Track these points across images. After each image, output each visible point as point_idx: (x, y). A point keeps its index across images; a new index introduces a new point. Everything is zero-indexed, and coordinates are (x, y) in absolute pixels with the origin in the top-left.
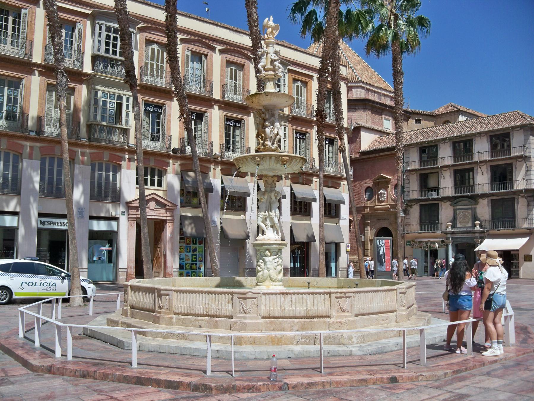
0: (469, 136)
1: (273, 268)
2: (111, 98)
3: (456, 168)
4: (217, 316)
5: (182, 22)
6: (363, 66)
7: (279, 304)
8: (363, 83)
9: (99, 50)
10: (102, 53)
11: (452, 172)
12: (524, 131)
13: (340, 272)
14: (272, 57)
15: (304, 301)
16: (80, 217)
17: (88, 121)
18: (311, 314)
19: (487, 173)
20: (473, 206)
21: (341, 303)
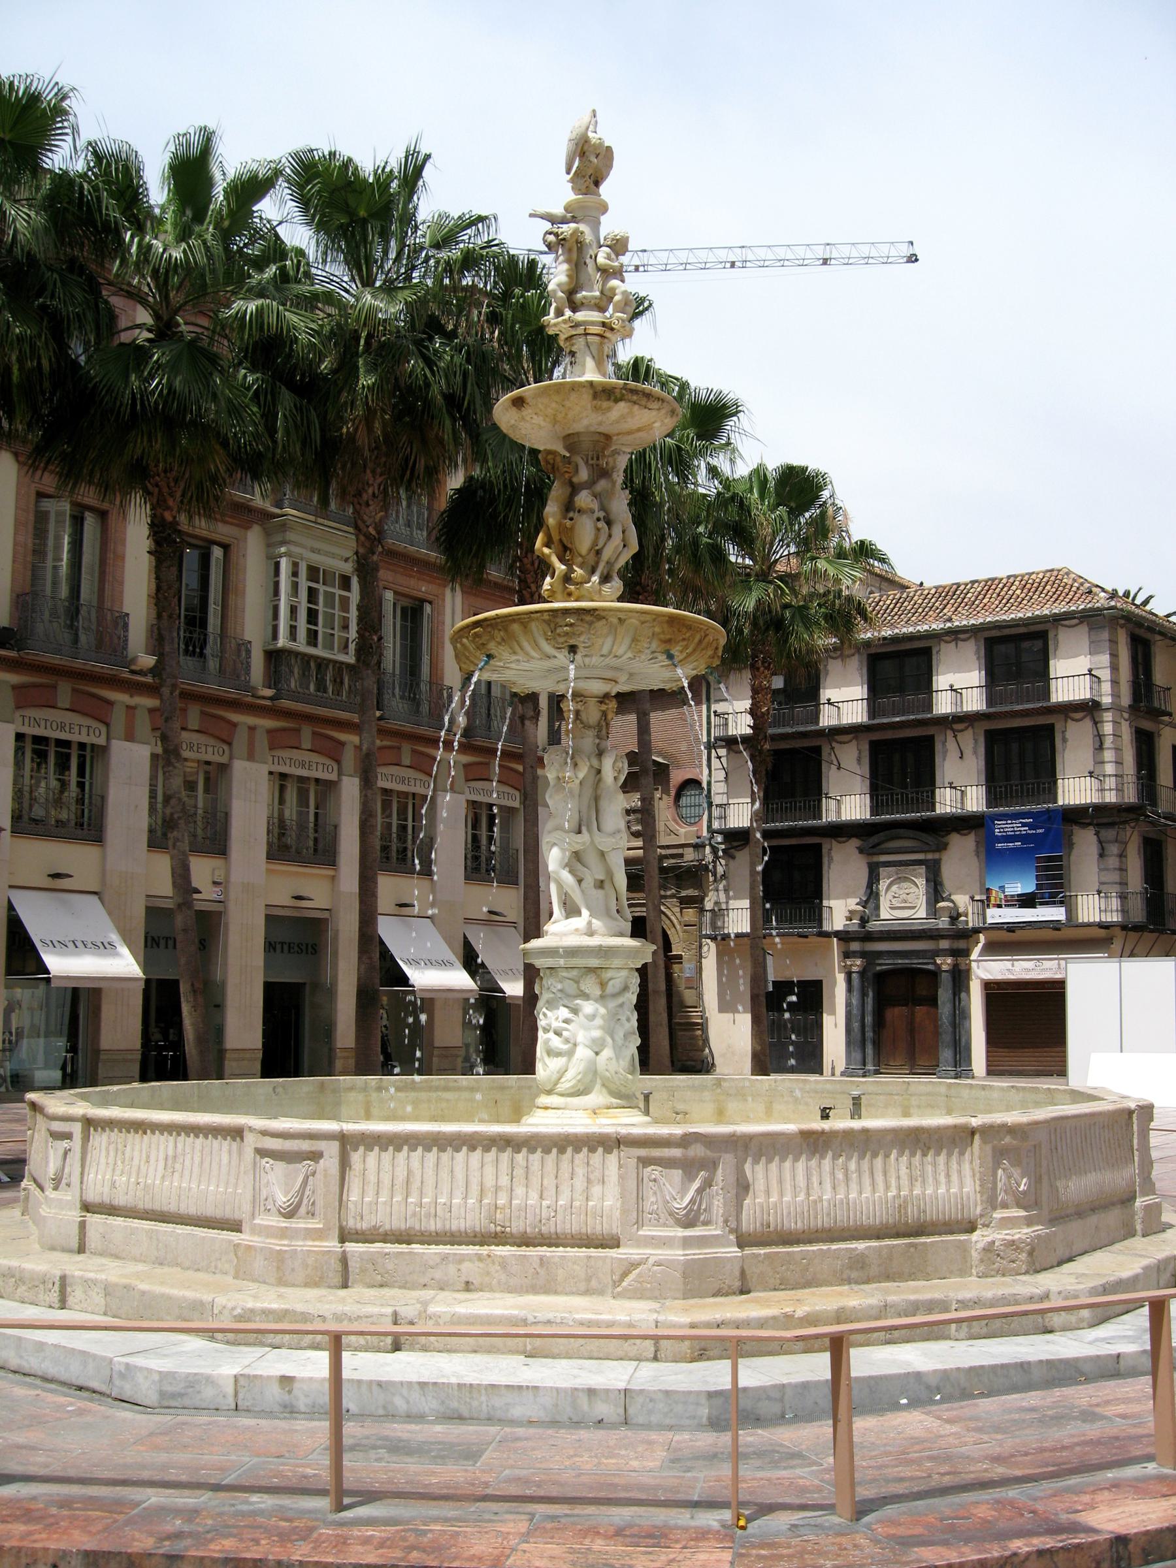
0: (1040, 623)
3: (877, 736)
4: (920, 1230)
11: (866, 747)
12: (1091, 629)
19: (975, 753)
20: (930, 856)
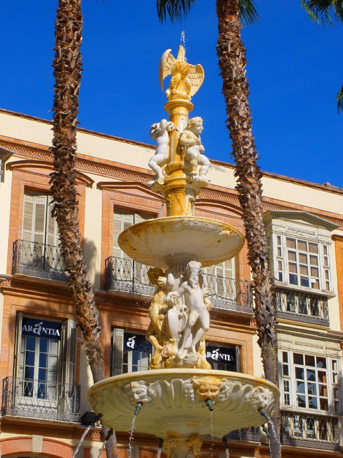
5: (88, 144)
14: (184, 139)
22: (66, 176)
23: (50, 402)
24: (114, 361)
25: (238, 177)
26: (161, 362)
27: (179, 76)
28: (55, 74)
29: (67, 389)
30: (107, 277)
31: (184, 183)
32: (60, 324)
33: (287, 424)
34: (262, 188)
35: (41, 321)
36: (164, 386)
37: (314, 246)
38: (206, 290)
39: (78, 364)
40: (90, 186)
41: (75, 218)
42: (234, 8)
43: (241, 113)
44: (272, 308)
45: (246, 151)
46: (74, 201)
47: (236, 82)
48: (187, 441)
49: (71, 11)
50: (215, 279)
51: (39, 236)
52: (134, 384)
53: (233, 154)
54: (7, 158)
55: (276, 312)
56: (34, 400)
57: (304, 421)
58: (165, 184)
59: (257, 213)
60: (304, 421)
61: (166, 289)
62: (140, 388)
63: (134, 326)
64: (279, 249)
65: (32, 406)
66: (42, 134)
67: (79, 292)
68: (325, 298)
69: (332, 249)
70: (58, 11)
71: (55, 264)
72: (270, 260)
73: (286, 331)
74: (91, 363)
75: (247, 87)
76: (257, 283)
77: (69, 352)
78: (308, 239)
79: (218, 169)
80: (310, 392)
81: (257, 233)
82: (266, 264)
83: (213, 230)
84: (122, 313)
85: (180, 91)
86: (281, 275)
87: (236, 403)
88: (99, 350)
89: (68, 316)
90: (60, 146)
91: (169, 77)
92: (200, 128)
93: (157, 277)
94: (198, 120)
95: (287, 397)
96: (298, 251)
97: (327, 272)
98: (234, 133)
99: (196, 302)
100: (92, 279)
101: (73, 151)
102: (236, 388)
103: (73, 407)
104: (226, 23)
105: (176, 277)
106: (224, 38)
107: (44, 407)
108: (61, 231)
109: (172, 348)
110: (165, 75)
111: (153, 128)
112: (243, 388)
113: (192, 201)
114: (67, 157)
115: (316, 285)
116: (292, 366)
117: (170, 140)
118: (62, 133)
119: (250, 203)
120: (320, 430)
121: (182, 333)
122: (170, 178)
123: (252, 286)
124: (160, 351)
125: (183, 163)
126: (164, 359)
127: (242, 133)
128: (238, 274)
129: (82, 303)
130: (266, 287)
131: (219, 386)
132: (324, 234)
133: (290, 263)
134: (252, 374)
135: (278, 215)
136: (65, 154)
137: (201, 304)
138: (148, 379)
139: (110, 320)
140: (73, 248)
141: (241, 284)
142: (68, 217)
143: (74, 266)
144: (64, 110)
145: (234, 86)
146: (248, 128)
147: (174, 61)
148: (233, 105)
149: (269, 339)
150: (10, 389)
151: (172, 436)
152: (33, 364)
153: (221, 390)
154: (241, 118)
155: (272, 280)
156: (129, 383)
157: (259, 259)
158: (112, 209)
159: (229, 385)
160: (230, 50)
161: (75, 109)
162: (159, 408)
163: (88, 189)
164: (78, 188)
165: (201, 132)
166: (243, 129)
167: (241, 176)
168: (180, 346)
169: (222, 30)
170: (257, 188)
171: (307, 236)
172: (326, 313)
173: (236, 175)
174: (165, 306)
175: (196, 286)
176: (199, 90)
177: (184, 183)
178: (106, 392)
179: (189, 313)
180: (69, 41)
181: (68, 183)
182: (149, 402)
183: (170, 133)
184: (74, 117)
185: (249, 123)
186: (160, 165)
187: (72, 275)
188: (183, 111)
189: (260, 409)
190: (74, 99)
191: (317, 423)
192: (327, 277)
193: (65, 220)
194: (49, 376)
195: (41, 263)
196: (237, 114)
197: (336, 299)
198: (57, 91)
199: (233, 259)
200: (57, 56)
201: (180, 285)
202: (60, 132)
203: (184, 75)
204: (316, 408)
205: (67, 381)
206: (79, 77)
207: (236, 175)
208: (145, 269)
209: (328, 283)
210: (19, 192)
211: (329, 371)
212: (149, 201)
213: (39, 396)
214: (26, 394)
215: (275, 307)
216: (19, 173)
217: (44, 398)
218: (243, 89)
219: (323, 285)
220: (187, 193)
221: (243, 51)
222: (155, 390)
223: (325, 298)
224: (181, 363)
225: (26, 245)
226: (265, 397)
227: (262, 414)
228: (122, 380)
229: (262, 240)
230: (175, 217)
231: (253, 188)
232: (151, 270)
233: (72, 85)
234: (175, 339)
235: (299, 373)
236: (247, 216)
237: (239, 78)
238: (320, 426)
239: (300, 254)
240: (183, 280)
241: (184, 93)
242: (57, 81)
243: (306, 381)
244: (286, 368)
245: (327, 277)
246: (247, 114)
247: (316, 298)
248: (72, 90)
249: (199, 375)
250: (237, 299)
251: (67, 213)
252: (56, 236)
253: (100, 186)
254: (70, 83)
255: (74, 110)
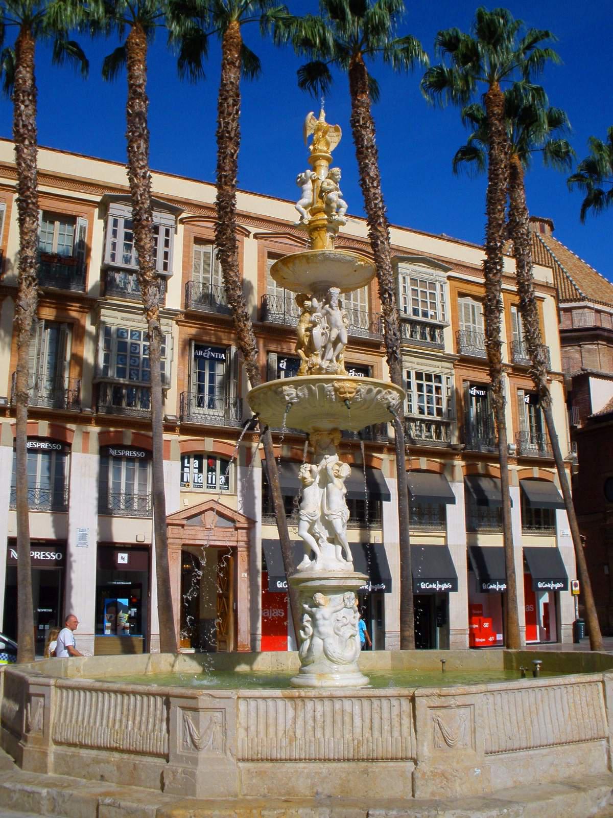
1: (332, 633)
2: (134, 337)
5: (245, 202)
6: (588, 274)
7: (281, 728)
8: (590, 300)
9: (113, 257)
10: (119, 263)
13: (388, 641)
14: (325, 185)
15: (347, 719)
16: (80, 543)
17: (94, 378)
18: (364, 752)
21: (443, 724)
22: (228, 226)
23: (219, 412)
24: (268, 373)
25: (370, 227)
26: (307, 371)
27: (320, 133)
28: (218, 142)
29: (232, 401)
30: (263, 311)
31: (326, 223)
32: (225, 349)
33: (410, 428)
34: (390, 236)
35: (209, 347)
36: (310, 390)
37: (432, 285)
38: (344, 312)
39: (240, 381)
40: (248, 236)
41: (236, 261)
42: (364, 88)
43: (372, 174)
44: (398, 333)
45: (376, 204)
46: (234, 246)
47: (367, 148)
48: (329, 434)
49: (231, 90)
50: (351, 312)
51: (206, 277)
52: (285, 388)
53: (366, 207)
54: (180, 214)
55: (401, 338)
56: (205, 410)
57: (423, 425)
58: (309, 224)
59: (386, 256)
60: (423, 425)
61: (311, 311)
62: (290, 392)
63: (285, 351)
64: (404, 287)
65: (204, 414)
66: (208, 194)
67: (240, 321)
68: (441, 327)
69: (447, 288)
70: (220, 90)
71: (220, 299)
72: (396, 294)
73: (409, 354)
74: (251, 379)
75: (376, 153)
76: (386, 314)
77: (233, 371)
78: (428, 279)
79: (354, 222)
80: (428, 403)
81: (386, 272)
82: (393, 298)
83: (350, 261)
84: (274, 340)
85: (321, 146)
86: (405, 308)
87: (370, 403)
88: (257, 368)
89: (231, 343)
90: (222, 201)
91: (312, 135)
92: (339, 177)
93: (303, 301)
94: (337, 170)
95: (410, 407)
96: (419, 289)
97: (443, 306)
98: (366, 190)
99: (336, 322)
100: (250, 310)
101: (234, 205)
102: (370, 391)
103: (236, 416)
104: (358, 100)
105: (319, 300)
106: (357, 112)
107: (213, 415)
108: (224, 271)
109: (316, 359)
110: (309, 133)
111: (298, 178)
112: (375, 390)
113: (332, 238)
114: (229, 210)
115: (434, 317)
116: (414, 382)
117: (314, 187)
118: (224, 190)
119: (380, 248)
120: (436, 432)
121: (325, 347)
122: (314, 218)
123: (382, 317)
124: (307, 362)
125: (324, 206)
126: (310, 369)
127: (373, 191)
128: (370, 309)
129: (242, 330)
130: (394, 317)
131: (355, 389)
132: (441, 275)
133: (413, 299)
134: (382, 378)
135: (403, 260)
136: (227, 208)
137: (340, 323)
138: (297, 384)
139: (265, 346)
140: (235, 286)
141: (373, 316)
142: (230, 260)
143: (235, 300)
144: (225, 171)
145: (365, 152)
146: (378, 186)
147: (316, 121)
148: (365, 167)
149: (396, 359)
150: (186, 402)
151: (317, 430)
152: (204, 382)
153: (357, 392)
154: (371, 178)
155: (398, 311)
156: (281, 387)
157: (387, 293)
158: (266, 255)
159: (363, 389)
160: (361, 122)
161: (235, 171)
162: (305, 408)
163: (246, 239)
164: (238, 237)
165: (339, 180)
166: (374, 187)
167: (372, 226)
168: (323, 357)
169: (355, 106)
170: (386, 235)
171: (426, 276)
172: (442, 339)
173: (368, 225)
174: (311, 325)
175: (336, 309)
176: (338, 146)
177: (326, 223)
178: (262, 395)
179: (330, 330)
180: (230, 114)
181: (229, 231)
182: (298, 403)
183: (313, 181)
184: (234, 177)
185: (379, 182)
186: (306, 208)
187: (234, 307)
188: (324, 163)
189: (389, 407)
190: (234, 162)
191: (433, 427)
192: (443, 310)
193: (228, 262)
194: (217, 390)
195: (207, 298)
196: (368, 174)
197: (450, 327)
198: (220, 156)
199: (366, 287)
200: (220, 127)
201: (322, 308)
202: (223, 190)
203: (325, 133)
204: (433, 415)
205: (232, 395)
206: (238, 144)
207: (368, 225)
208: (293, 295)
209: (443, 315)
210: (189, 242)
211: (443, 386)
212: (297, 248)
213: (209, 407)
214: (199, 406)
215: (401, 333)
216: (190, 226)
217: (213, 408)
218: (373, 154)
219: (440, 317)
220: (328, 231)
221: (373, 123)
222: (303, 392)
223: (441, 327)
224: (324, 371)
225: (196, 285)
226: (393, 398)
227: (391, 412)
228: (275, 385)
229: (390, 278)
230: (318, 250)
231: (382, 236)
232: (298, 296)
233: (232, 151)
234: (319, 352)
235: (420, 387)
236: (377, 258)
237: (369, 145)
238: (436, 429)
239: (421, 291)
240: (325, 304)
241: (325, 149)
242: (220, 148)
243: (425, 393)
244: (409, 384)
245: (443, 310)
246: (376, 175)
247: (434, 327)
248: (232, 155)
249: (339, 380)
250: (370, 329)
251: (229, 256)
252: (221, 279)
253: (256, 236)
254: (230, 149)
255: (233, 171)
